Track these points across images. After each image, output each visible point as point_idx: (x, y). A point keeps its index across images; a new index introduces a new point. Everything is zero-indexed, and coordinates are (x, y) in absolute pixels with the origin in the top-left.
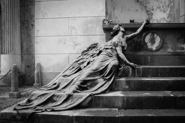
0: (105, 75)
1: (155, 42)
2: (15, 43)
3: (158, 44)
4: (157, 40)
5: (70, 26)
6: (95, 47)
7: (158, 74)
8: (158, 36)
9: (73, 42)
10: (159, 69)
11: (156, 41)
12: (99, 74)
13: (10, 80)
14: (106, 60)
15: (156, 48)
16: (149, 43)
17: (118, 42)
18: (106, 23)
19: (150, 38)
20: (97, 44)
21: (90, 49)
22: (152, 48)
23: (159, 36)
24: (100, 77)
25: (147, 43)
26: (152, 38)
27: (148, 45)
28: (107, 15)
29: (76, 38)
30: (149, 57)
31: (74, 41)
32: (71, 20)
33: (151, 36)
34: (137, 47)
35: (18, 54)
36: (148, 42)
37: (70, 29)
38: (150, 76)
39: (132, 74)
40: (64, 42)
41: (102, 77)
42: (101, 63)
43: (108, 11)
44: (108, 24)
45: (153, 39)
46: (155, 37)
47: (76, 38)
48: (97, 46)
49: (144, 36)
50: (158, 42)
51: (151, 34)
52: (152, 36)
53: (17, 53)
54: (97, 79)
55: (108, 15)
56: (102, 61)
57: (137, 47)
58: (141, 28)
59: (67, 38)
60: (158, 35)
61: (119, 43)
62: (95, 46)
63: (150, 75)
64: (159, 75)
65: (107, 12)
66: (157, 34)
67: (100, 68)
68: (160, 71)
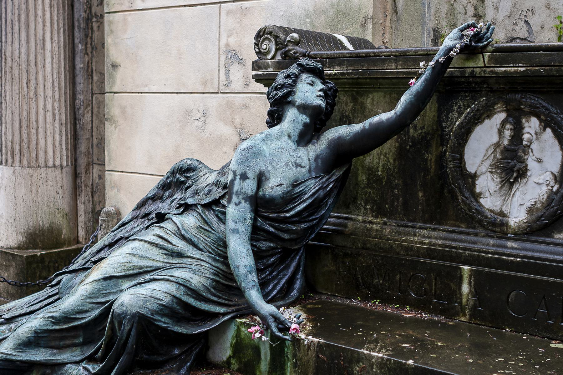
1: (523, 173)
2: (37, 121)
3: (545, 189)
4: (540, 161)
6: (183, 183)
8: (548, 130)
11: (531, 163)
12: (81, 340)
15: (530, 210)
16: (488, 174)
17: (234, 172)
18: (268, 52)
19: (497, 145)
20: (190, 169)
21: (167, 194)
22: (504, 209)
23: (555, 132)
24: (79, 358)
25: (474, 177)
26: (506, 142)
27: (478, 190)
30: (466, 268)
33: (500, 132)
35: (51, 163)
36: (483, 169)
37: (223, 58)
44: (278, 58)
45: (516, 151)
46: (526, 136)
48: (188, 178)
49: (460, 126)
50: (548, 176)
51: (503, 115)
52: (507, 133)
53: (46, 160)
54: (65, 364)
56: (105, 279)
58: (416, 85)
59: (214, 101)
60: (546, 124)
61: (237, 182)
66: (538, 117)
67: (86, 311)
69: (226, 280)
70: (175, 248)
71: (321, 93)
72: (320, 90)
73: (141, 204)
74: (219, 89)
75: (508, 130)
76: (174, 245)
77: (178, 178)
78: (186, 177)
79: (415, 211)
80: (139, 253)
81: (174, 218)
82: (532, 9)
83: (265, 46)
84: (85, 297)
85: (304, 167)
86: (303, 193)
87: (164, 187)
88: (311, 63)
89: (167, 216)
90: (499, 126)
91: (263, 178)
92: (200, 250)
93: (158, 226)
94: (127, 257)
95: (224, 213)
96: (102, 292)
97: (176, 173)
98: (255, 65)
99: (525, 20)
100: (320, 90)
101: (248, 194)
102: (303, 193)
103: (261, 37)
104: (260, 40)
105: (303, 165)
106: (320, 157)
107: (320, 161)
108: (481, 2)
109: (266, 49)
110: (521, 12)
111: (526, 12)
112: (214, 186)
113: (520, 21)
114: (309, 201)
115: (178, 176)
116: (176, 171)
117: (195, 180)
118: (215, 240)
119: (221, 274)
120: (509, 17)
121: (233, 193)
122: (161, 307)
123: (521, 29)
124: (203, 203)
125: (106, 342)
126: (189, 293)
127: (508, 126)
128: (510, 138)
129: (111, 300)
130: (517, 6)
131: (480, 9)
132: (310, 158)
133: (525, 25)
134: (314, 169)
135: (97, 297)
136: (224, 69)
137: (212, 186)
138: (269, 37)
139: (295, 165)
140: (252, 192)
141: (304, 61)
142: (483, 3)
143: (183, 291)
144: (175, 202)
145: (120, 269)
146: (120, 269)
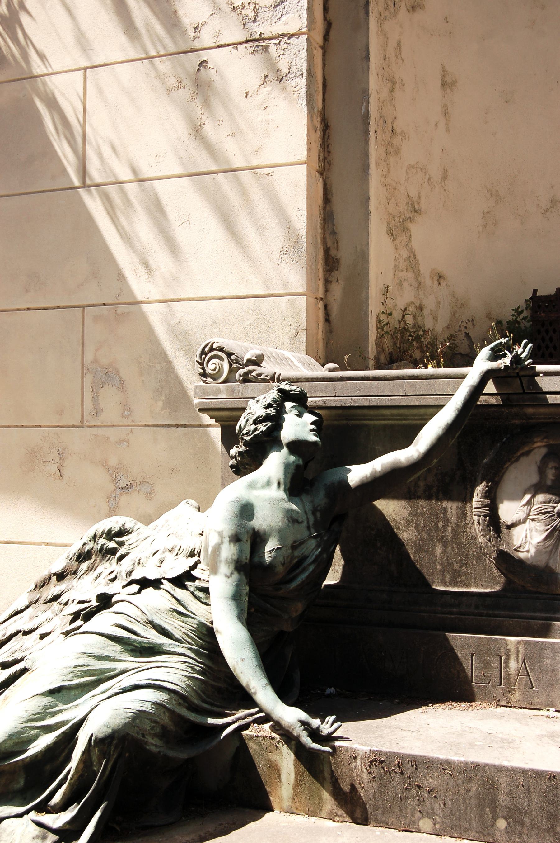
0: (57, 798)
5: (89, 357)
6: (113, 552)
7: (495, 819)
9: (104, 464)
10: (503, 781)
13: (354, 481)
14: (99, 682)
28: (335, 274)
29: (123, 441)
31: (113, 462)
32: (96, 319)
34: (439, 550)
37: (89, 379)
38: (426, 824)
39: (295, 788)
40: (53, 468)
41: (34, 808)
42: (48, 700)
43: (342, 244)
47: (123, 441)
48: (121, 544)
55: (341, 275)
57: (439, 550)
62: (112, 545)
63: (431, 815)
64: (502, 824)
65: (333, 253)
68: (510, 794)
69: (214, 680)
70: (145, 640)
71: (313, 427)
72: (312, 424)
73: (41, 582)
74: (82, 422)
75: (551, 468)
76: (143, 637)
77: (104, 544)
78: (117, 543)
79: (432, 573)
80: (97, 652)
81: (132, 598)
82: (473, 320)
83: (214, 366)
84: (25, 719)
85: (302, 522)
86: (304, 558)
87: (79, 557)
88: (294, 388)
89: (114, 599)
90: (539, 463)
91: (258, 540)
92: (177, 640)
93: (186, 608)
94: (78, 658)
95: (206, 590)
96: (48, 711)
97: (100, 537)
98: (198, 390)
99: (466, 332)
100: (312, 424)
101: (241, 561)
102: (305, 558)
103: (206, 355)
104: (204, 359)
105: (300, 520)
106: (319, 508)
107: (318, 515)
108: (419, 310)
109: (214, 370)
110: (460, 323)
111: (467, 323)
112: (168, 553)
113: (460, 333)
114: (311, 568)
115: (102, 541)
116: (99, 535)
117: (132, 546)
118: (195, 626)
119: (208, 672)
120: (448, 328)
121: (221, 561)
122: (153, 724)
123: (462, 343)
124: (170, 576)
125: (72, 781)
126: (180, 701)
127: (551, 464)
128: (553, 478)
129: (70, 721)
130: (457, 315)
131: (419, 318)
132: (307, 510)
133: (465, 339)
134: (313, 525)
135: (42, 719)
136: (90, 393)
137: (164, 552)
138: (220, 353)
139: (291, 521)
140: (246, 559)
141: (285, 386)
142: (421, 311)
143: (175, 700)
144: (102, 576)
145: (71, 675)
146: (71, 675)
